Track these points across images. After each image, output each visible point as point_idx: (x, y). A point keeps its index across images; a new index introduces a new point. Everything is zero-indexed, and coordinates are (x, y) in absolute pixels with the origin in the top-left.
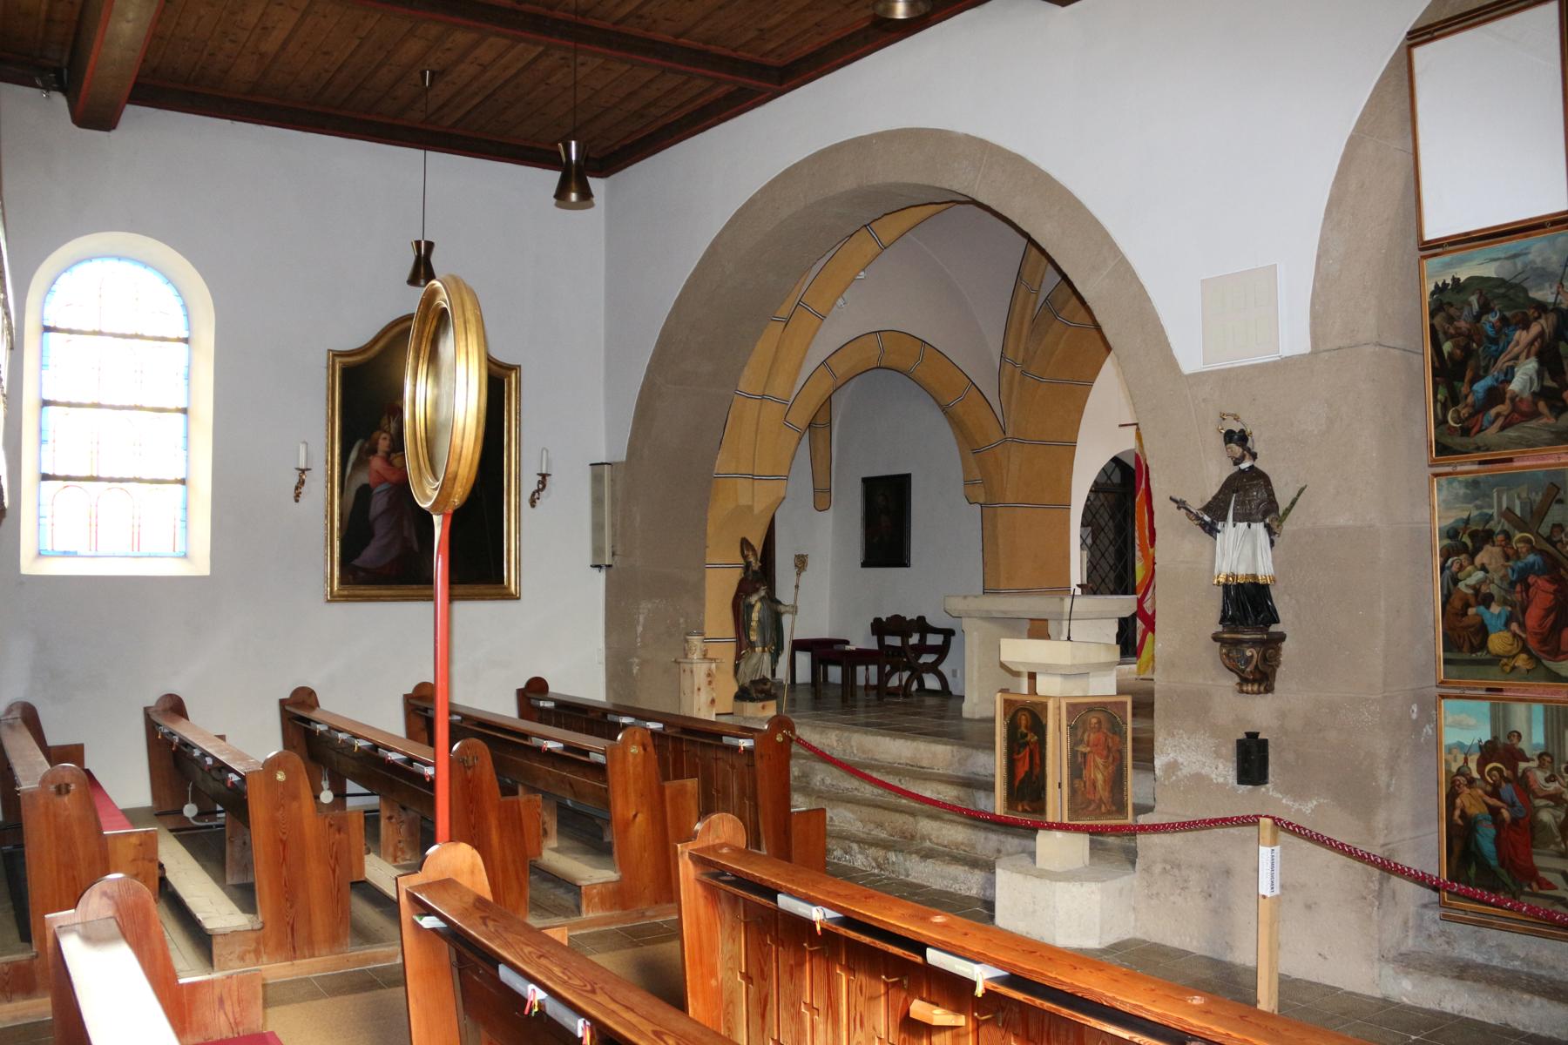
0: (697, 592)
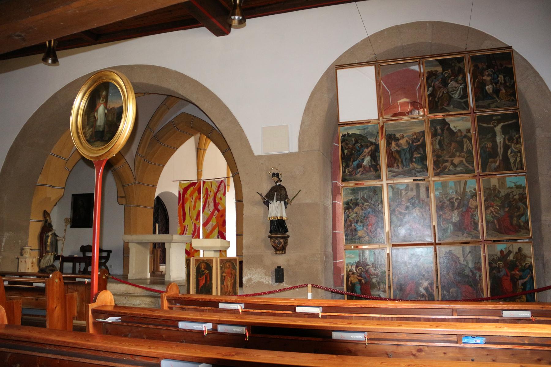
0: (26, 230)
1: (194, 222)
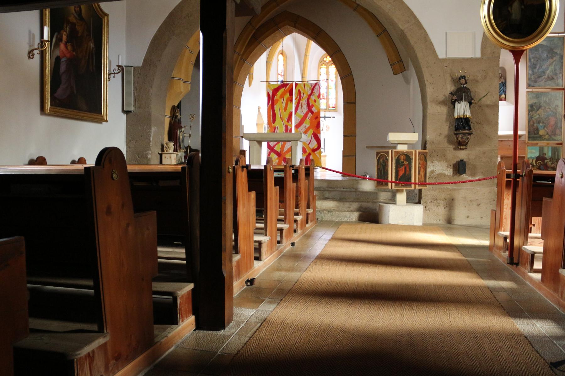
1: (286, 123)
